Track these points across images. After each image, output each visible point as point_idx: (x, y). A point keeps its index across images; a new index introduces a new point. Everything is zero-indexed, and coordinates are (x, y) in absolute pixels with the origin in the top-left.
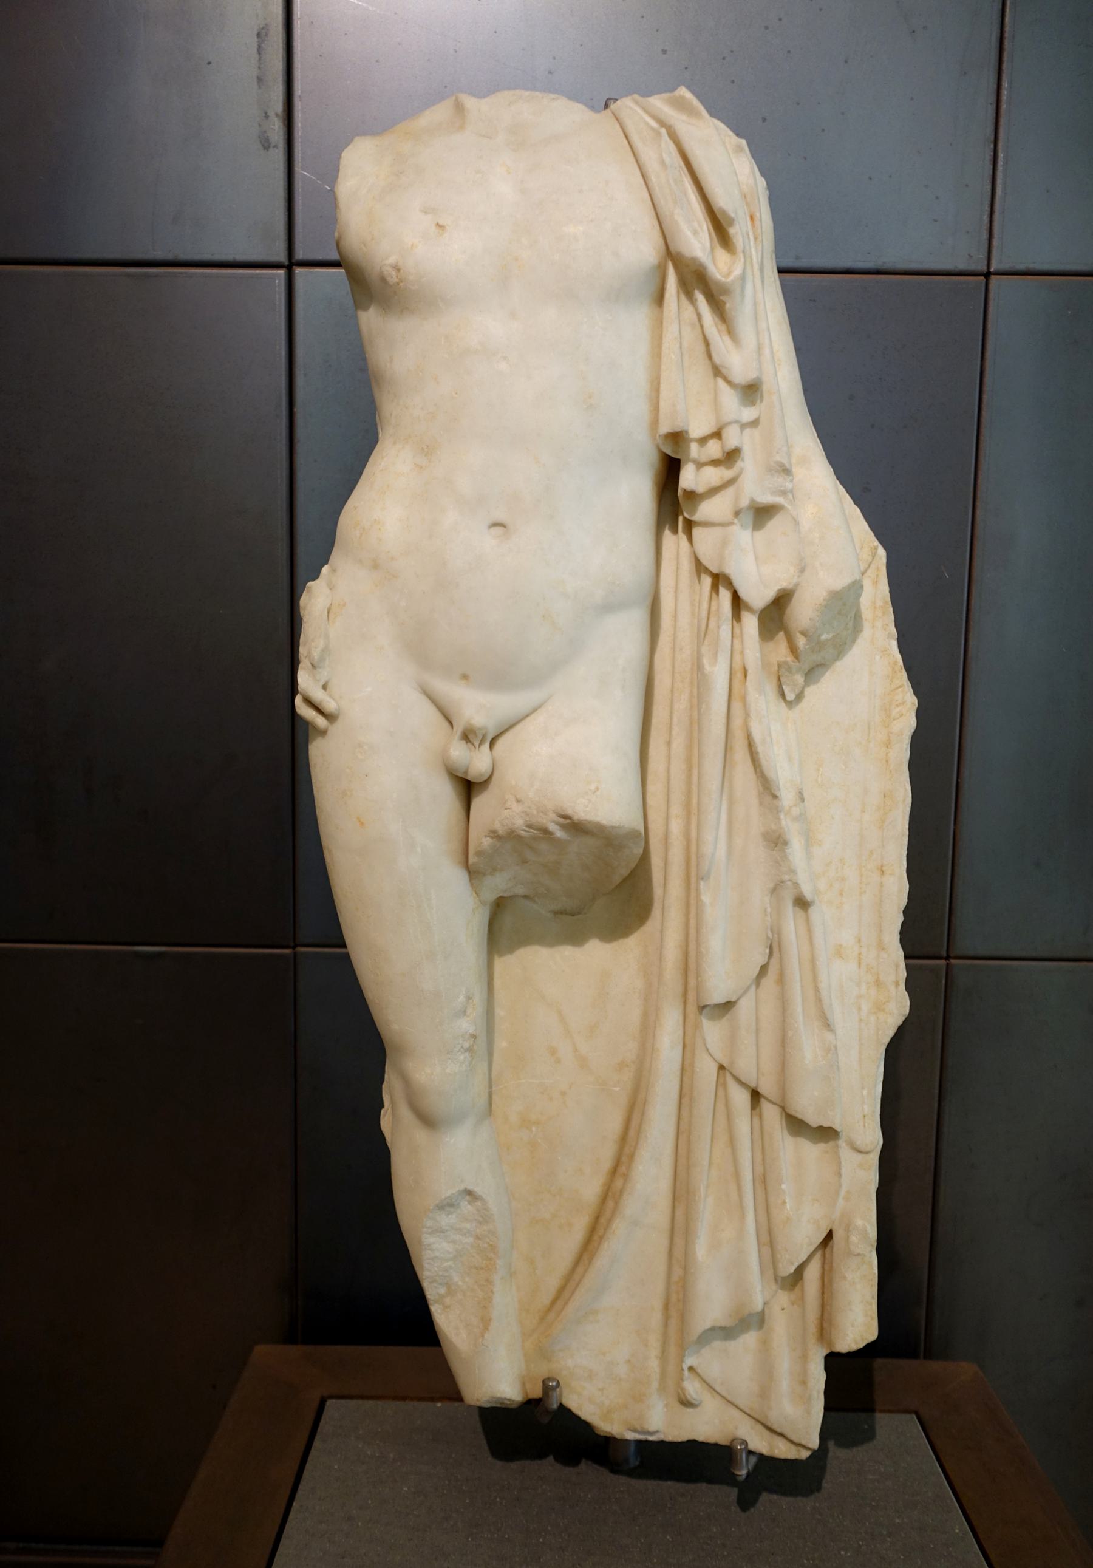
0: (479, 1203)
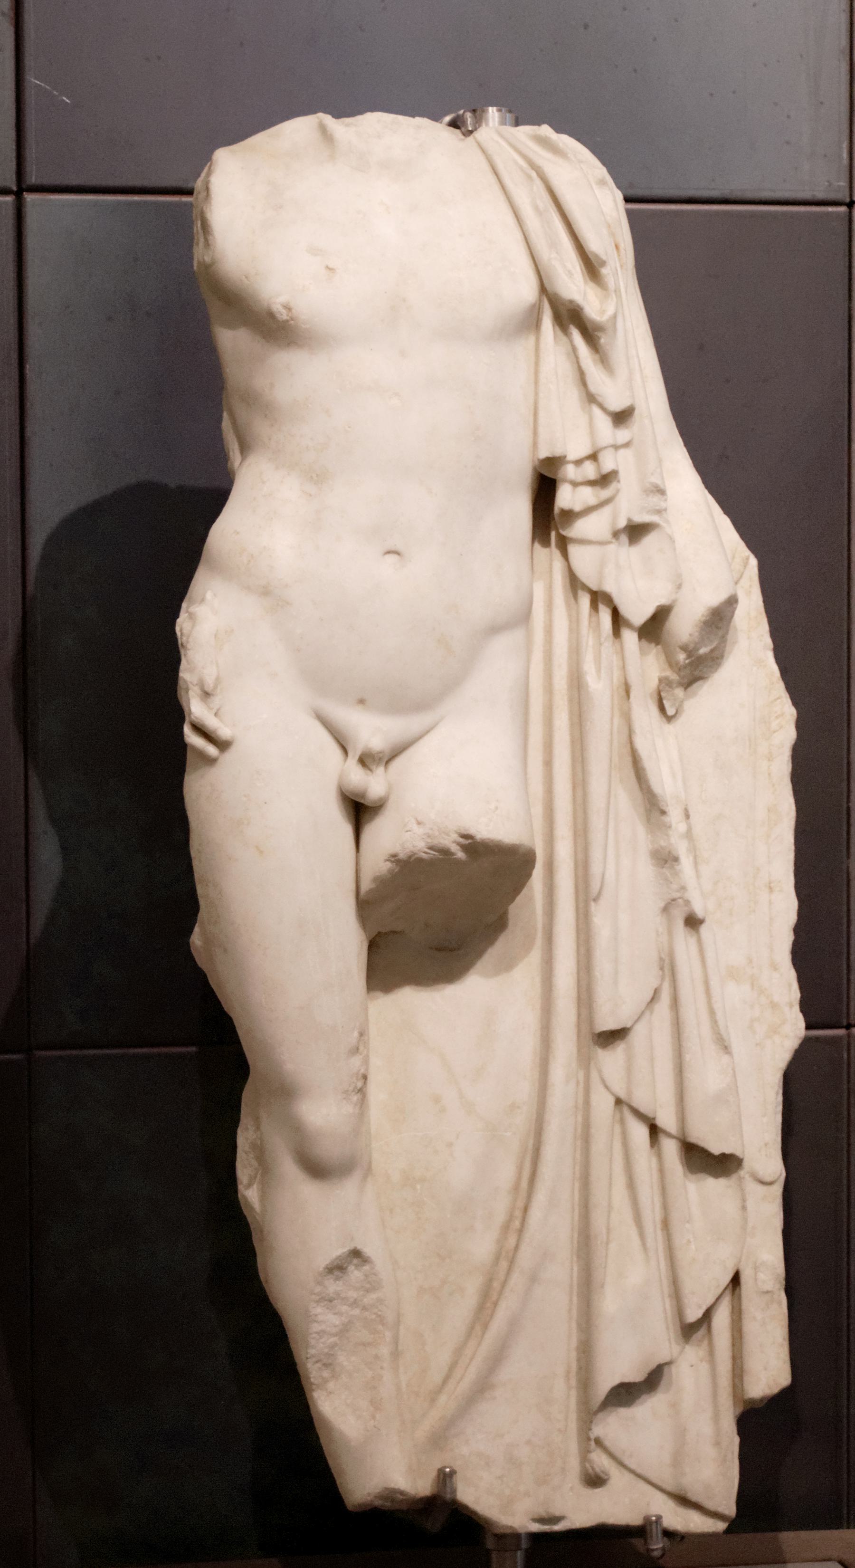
0: (366, 1268)
